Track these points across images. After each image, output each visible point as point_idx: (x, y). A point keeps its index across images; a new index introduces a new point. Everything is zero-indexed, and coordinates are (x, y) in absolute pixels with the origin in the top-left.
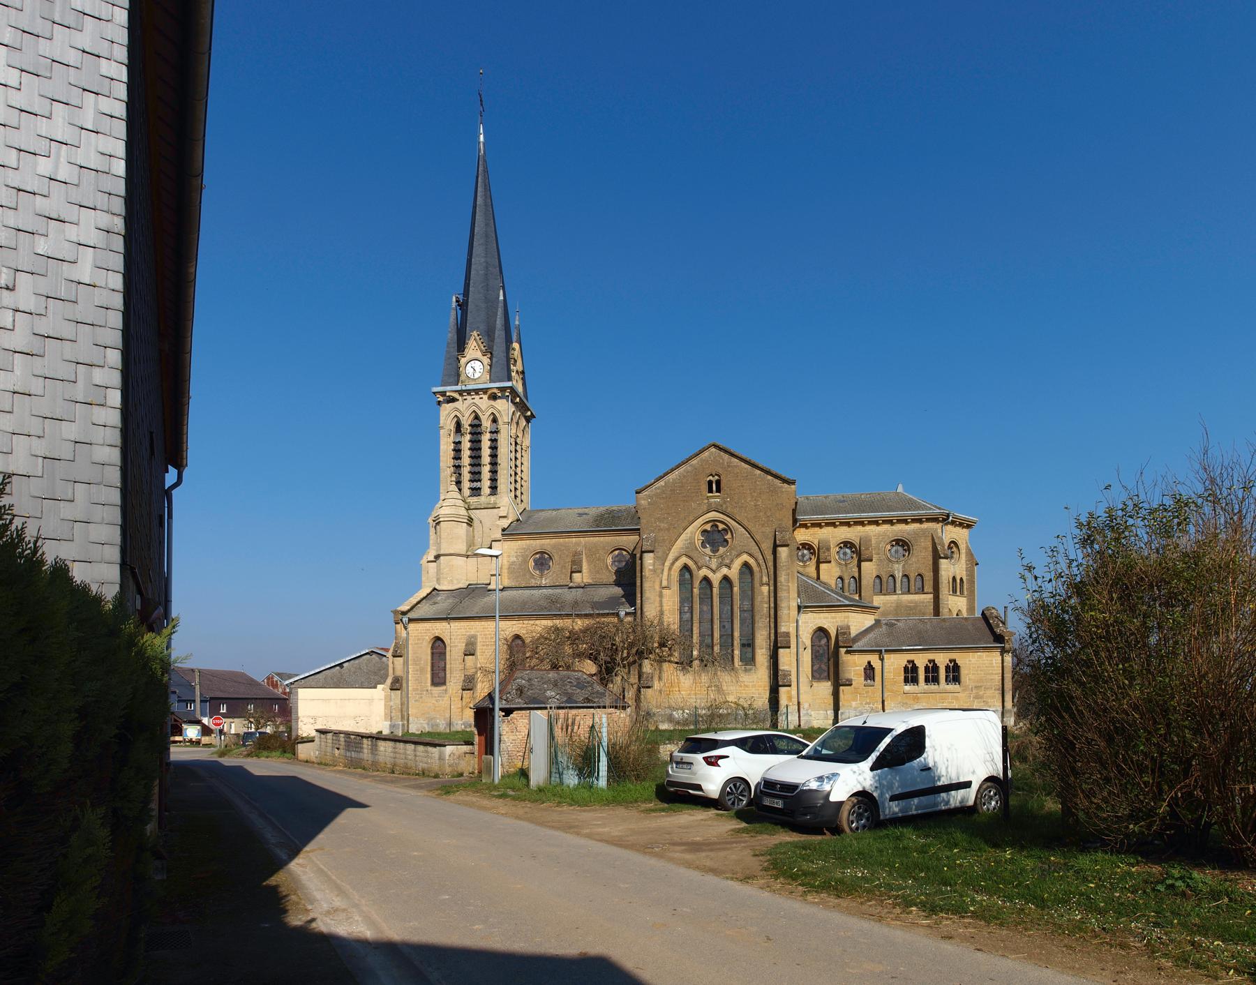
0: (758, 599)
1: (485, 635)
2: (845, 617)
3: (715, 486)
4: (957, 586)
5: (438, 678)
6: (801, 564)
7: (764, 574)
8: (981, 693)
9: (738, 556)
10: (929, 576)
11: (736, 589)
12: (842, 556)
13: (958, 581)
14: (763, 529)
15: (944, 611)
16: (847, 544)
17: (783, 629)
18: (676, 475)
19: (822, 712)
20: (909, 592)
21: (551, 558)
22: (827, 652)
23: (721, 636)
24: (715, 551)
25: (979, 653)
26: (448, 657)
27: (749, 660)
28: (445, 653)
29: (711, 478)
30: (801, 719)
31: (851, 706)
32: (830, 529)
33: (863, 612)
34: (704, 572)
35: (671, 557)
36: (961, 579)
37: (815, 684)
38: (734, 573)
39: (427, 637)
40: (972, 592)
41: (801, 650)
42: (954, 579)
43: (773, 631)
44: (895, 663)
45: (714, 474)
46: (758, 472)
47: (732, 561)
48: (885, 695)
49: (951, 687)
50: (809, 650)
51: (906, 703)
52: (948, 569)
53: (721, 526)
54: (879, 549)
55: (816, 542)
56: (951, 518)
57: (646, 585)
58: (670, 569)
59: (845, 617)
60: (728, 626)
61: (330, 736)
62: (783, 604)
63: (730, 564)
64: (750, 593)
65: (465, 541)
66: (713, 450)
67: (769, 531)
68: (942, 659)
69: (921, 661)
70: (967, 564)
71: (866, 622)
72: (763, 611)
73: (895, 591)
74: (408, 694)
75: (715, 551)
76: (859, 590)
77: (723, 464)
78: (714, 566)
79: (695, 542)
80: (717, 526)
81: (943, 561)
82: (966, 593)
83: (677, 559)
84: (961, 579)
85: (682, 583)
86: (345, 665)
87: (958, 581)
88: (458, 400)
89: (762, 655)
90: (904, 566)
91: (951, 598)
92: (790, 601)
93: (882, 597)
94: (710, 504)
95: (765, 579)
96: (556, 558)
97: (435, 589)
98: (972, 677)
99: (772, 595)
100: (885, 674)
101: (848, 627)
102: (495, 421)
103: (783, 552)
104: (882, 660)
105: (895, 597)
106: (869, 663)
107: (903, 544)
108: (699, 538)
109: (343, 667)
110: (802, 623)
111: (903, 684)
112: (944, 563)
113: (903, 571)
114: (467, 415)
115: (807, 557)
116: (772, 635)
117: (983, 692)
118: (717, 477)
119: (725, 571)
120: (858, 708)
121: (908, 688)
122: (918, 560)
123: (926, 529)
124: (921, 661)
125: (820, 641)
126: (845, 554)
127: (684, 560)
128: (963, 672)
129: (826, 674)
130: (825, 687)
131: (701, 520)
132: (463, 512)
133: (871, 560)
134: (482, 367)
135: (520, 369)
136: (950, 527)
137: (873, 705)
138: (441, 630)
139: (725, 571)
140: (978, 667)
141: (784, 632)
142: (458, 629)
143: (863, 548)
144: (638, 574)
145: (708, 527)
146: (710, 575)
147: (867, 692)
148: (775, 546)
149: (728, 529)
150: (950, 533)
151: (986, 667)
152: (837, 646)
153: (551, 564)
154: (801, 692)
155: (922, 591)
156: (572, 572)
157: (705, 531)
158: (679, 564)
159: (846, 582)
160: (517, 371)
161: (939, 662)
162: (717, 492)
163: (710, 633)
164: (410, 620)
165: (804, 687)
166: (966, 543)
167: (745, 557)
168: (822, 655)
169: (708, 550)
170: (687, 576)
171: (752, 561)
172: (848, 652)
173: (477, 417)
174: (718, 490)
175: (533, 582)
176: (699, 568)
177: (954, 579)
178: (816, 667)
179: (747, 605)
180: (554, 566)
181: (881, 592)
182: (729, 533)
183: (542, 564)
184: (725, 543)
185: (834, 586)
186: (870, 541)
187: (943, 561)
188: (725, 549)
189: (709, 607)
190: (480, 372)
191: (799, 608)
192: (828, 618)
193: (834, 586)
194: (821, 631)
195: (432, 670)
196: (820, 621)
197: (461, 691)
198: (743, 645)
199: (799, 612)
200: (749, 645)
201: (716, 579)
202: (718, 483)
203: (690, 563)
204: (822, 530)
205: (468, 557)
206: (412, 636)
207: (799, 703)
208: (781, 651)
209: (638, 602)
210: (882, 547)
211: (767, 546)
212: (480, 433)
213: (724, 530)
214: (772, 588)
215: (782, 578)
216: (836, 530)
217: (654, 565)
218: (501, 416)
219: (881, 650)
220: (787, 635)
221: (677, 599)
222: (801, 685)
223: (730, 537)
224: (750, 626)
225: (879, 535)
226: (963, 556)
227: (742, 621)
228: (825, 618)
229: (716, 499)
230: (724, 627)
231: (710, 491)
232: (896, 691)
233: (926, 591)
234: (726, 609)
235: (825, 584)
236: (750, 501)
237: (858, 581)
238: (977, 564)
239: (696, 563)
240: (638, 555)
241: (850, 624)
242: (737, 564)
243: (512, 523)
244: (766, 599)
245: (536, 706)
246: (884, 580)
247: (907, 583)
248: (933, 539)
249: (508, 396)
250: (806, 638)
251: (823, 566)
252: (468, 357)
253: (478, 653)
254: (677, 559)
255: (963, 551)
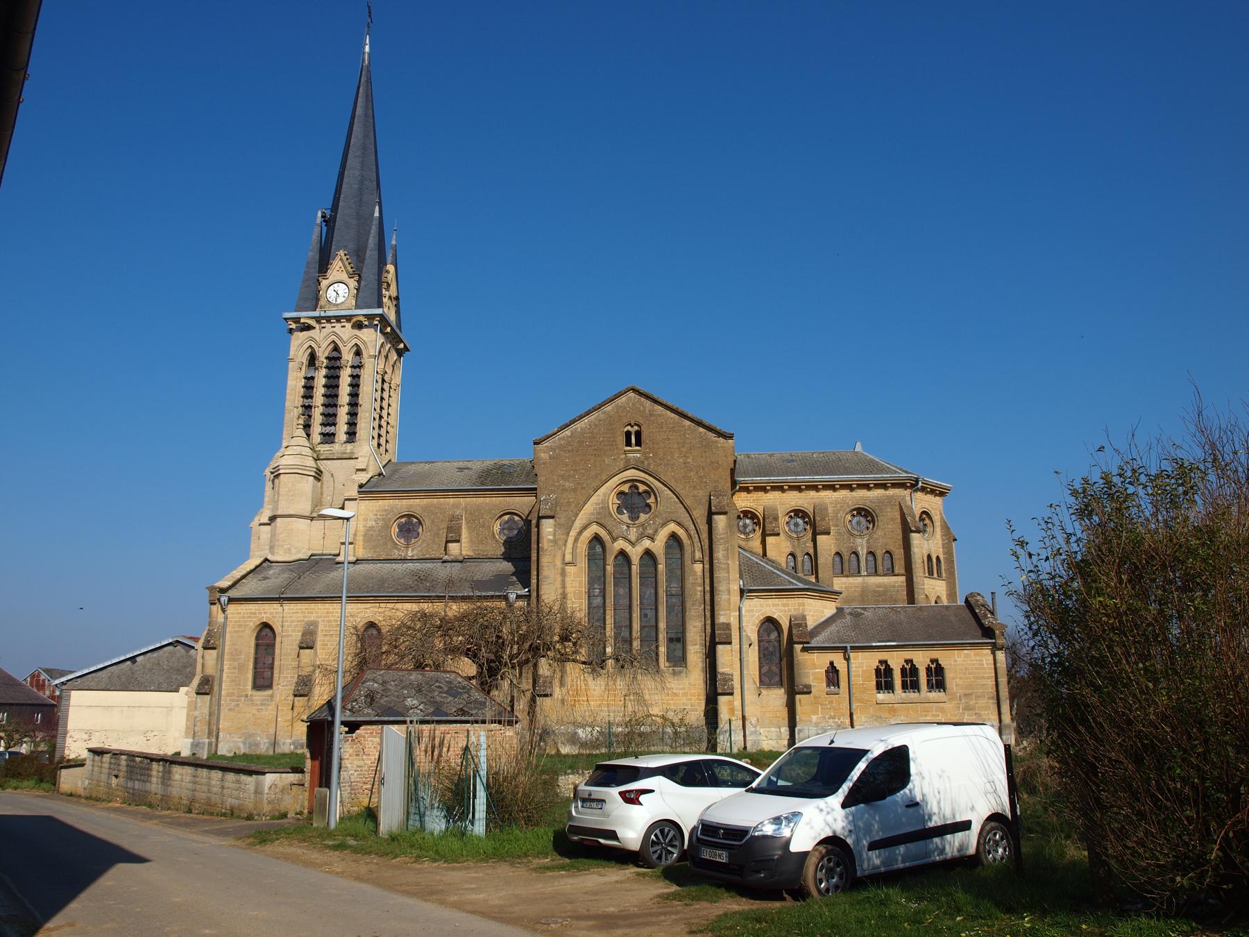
0: (689, 581)
1: (328, 621)
2: (800, 605)
3: (635, 438)
4: (933, 566)
5: (263, 680)
6: (743, 536)
7: (696, 548)
8: (972, 703)
9: (664, 525)
10: (899, 554)
11: (661, 567)
12: (792, 527)
13: (934, 560)
14: (695, 492)
15: (920, 597)
16: (798, 513)
17: (721, 619)
18: (585, 423)
19: (773, 729)
20: (876, 573)
21: (420, 523)
22: (777, 649)
23: (642, 628)
24: (634, 518)
25: (965, 651)
26: (277, 651)
27: (679, 660)
28: (274, 645)
29: (629, 428)
30: (748, 738)
31: (811, 721)
32: (777, 494)
33: (822, 598)
34: (620, 544)
35: (578, 524)
36: (938, 558)
37: (764, 692)
38: (658, 546)
39: (251, 624)
40: (951, 574)
41: (745, 646)
42: (929, 557)
43: (709, 622)
44: (864, 664)
45: (633, 424)
46: (688, 423)
47: (656, 531)
48: (854, 707)
49: (934, 695)
50: (755, 647)
51: (881, 717)
52: (923, 546)
53: (642, 488)
54: (837, 520)
55: (761, 510)
56: (920, 484)
57: (545, 560)
58: (576, 540)
59: (800, 605)
60: (651, 614)
61: (107, 758)
62: (721, 587)
63: (654, 535)
64: (679, 573)
65: (311, 498)
66: (632, 394)
67: (702, 494)
68: (921, 659)
69: (896, 661)
70: (943, 540)
71: (825, 610)
72: (696, 594)
73: (859, 572)
74: (219, 700)
75: (634, 518)
76: (815, 570)
77: (644, 411)
78: (633, 538)
79: (608, 506)
80: (637, 488)
81: (914, 536)
82: (944, 575)
83: (585, 528)
84: (938, 558)
85: (591, 558)
86: (139, 659)
87: (934, 560)
88: (314, 328)
89: (695, 654)
90: (868, 540)
91: (927, 581)
92: (729, 583)
93: (844, 579)
94: (627, 460)
95: (698, 555)
96: (427, 523)
97: (266, 560)
98: (960, 682)
99: (707, 575)
100: (852, 679)
101: (804, 618)
102: (358, 353)
103: (720, 521)
104: (847, 659)
105: (859, 580)
106: (832, 663)
107: (865, 514)
108: (613, 502)
109: (136, 661)
110: (745, 612)
111: (875, 691)
112: (915, 538)
113: (868, 547)
114: (324, 345)
115: (750, 528)
116: (708, 627)
117: (974, 701)
118: (636, 428)
119: (647, 543)
120: (819, 723)
121: (881, 696)
122: (885, 534)
123: (892, 496)
124: (896, 661)
125: (769, 635)
126: (796, 525)
127: (594, 528)
128: (949, 675)
129: (777, 678)
130: (777, 696)
131: (616, 480)
132: (311, 462)
133: (829, 533)
134: (347, 290)
135: (394, 294)
136: (919, 495)
137: (839, 719)
138: (272, 613)
139: (647, 543)
140: (966, 669)
141: (723, 623)
142: (293, 613)
143: (818, 518)
144: (534, 546)
145: (626, 488)
146: (628, 548)
147: (831, 702)
148: (710, 514)
149: (650, 491)
150: (920, 502)
151: (976, 668)
152: (791, 642)
153: (420, 530)
154: (747, 702)
155: (892, 572)
156: (447, 542)
157: (621, 493)
158: (588, 534)
159: (799, 559)
160: (390, 297)
161: (918, 662)
162: (636, 445)
163: (628, 623)
164: (231, 600)
165: (750, 696)
166: (941, 514)
167: (672, 527)
168: (772, 653)
169: (625, 517)
170: (598, 549)
171: (681, 532)
172: (804, 650)
173: (336, 349)
174: (638, 443)
175: (396, 554)
176: (614, 540)
177: (929, 557)
178: (765, 669)
179: (675, 587)
180: (425, 534)
181: (842, 573)
182: (653, 496)
183: (409, 531)
184: (647, 509)
185: (784, 565)
186: (826, 509)
187: (914, 536)
188: (647, 516)
189: (627, 590)
190: (344, 297)
191: (742, 592)
192: (778, 605)
193: (784, 565)
194: (770, 623)
195: (255, 668)
196: (768, 608)
197: (291, 697)
198: (670, 640)
199: (741, 597)
200: (678, 640)
201: (635, 553)
202: (638, 434)
203: (603, 533)
204: (768, 495)
205: (312, 519)
206: (231, 621)
207: (744, 718)
208: (720, 648)
209: (534, 581)
210: (841, 517)
211: (700, 513)
212: (339, 368)
213: (645, 492)
214: (707, 566)
215: (720, 554)
216: (784, 495)
217: (554, 535)
218: (366, 348)
219: (846, 647)
220: (727, 626)
221: (584, 579)
222: (746, 693)
223: (654, 501)
224: (680, 615)
225: (837, 502)
226: (938, 530)
227: (670, 609)
228: (774, 605)
229: (635, 453)
230: (646, 615)
231: (628, 443)
232: (868, 701)
233: (896, 572)
234: (648, 592)
235: (772, 562)
236: (678, 457)
237: (814, 558)
238: (955, 540)
239: (610, 533)
240: (534, 522)
241: (806, 613)
242: (663, 535)
243: (372, 477)
244: (700, 581)
245: (392, 719)
246: (846, 558)
247: (873, 562)
248: (901, 509)
249: (377, 325)
250: (751, 632)
251: (770, 540)
252: (331, 279)
253: (319, 645)
254: (585, 528)
255: (938, 524)
